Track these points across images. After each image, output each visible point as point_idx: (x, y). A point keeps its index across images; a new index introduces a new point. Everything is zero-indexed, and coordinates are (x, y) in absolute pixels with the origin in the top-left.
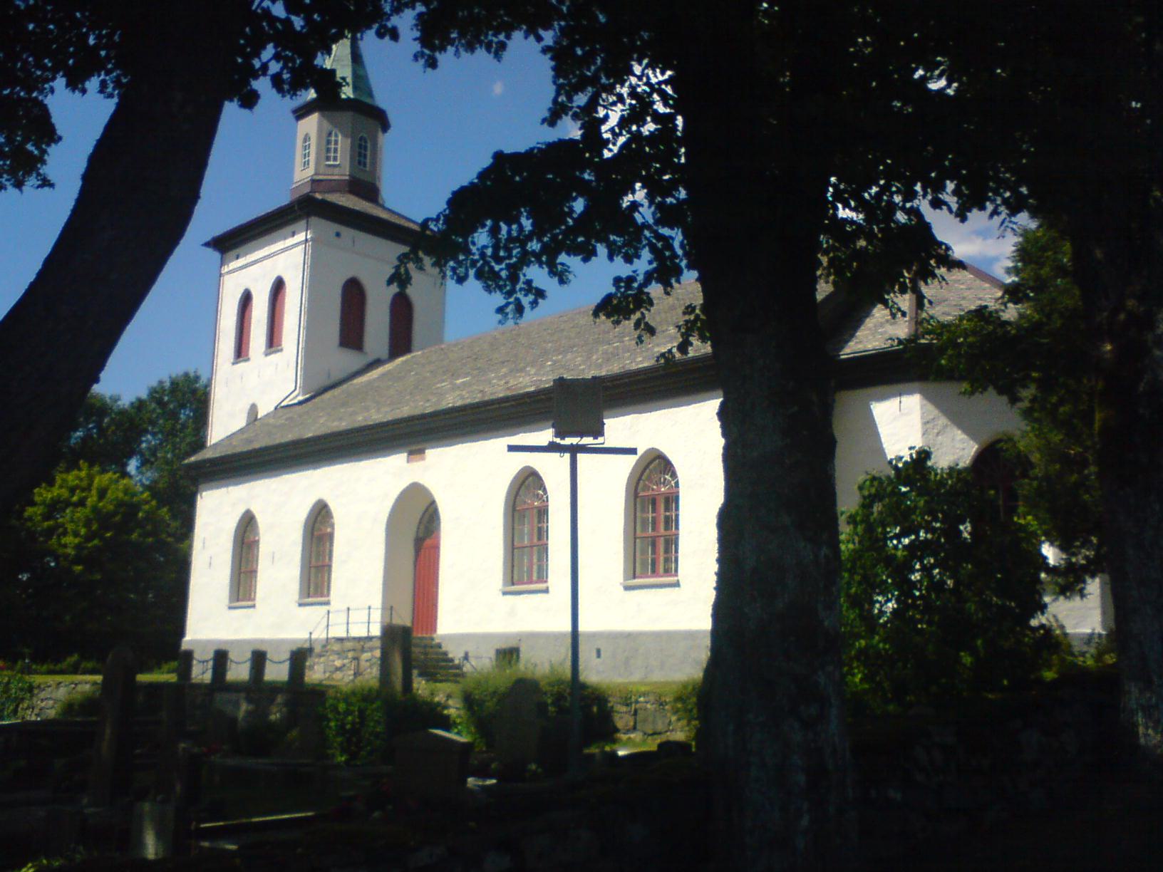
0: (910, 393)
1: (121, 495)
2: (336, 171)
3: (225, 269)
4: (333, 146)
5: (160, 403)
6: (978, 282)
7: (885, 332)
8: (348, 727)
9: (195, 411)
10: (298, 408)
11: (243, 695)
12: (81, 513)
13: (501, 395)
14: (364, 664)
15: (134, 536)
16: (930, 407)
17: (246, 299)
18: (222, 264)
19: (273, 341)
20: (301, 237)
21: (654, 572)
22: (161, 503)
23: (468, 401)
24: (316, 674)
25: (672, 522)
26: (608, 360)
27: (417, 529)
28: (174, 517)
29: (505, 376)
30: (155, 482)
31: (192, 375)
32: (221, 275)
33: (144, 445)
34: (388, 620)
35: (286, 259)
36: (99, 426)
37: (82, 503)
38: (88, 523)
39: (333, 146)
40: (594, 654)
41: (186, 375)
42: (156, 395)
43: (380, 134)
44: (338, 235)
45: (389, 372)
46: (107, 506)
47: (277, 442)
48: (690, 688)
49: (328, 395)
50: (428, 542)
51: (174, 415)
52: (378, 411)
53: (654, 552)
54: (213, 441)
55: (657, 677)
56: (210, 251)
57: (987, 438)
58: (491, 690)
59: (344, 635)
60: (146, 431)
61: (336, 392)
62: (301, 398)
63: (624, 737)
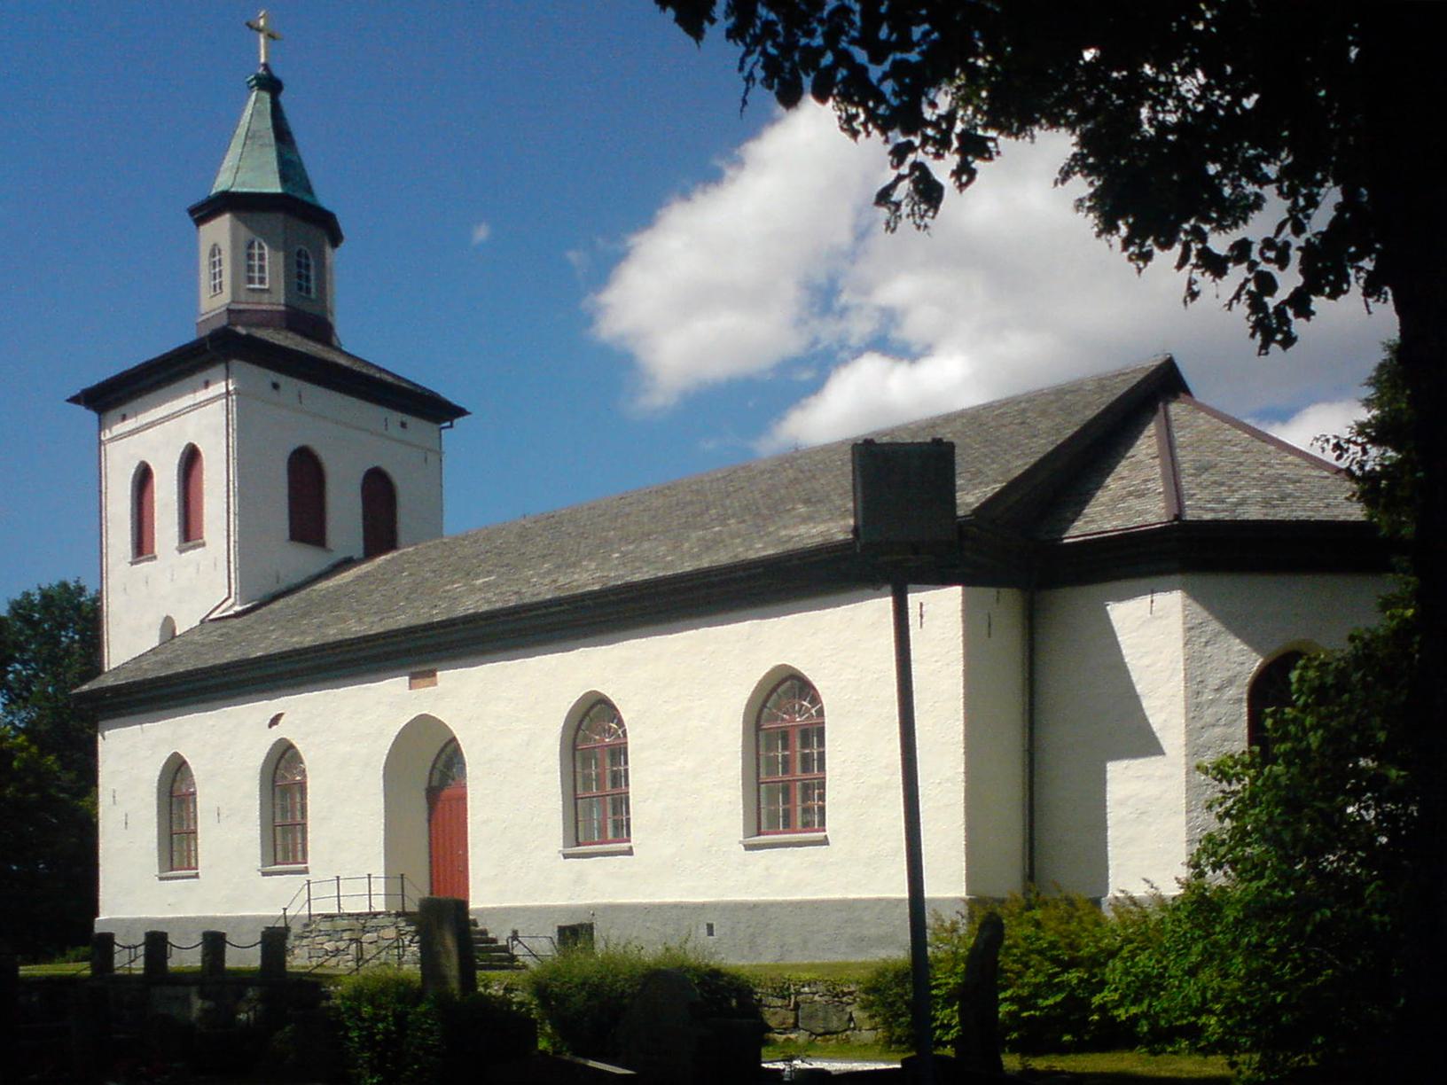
0: (1169, 589)
2: (266, 297)
3: (106, 435)
5: (27, 620)
6: (1258, 443)
7: (1129, 508)
9: (82, 633)
10: (236, 621)
11: (194, 989)
13: (549, 597)
16: (1196, 608)
17: (143, 477)
18: (101, 428)
19: (189, 532)
20: (219, 388)
21: (788, 826)
22: (45, 750)
23: (498, 605)
24: (299, 960)
26: (708, 548)
28: (66, 768)
29: (549, 572)
30: (32, 723)
31: (72, 585)
33: (11, 676)
34: (418, 891)
35: (200, 418)
40: (704, 931)
41: (64, 585)
43: (328, 250)
44: (276, 386)
45: (367, 574)
47: (210, 663)
48: (890, 975)
49: (276, 606)
50: (447, 792)
53: (786, 800)
54: (113, 666)
55: (797, 958)
56: (80, 409)
57: (1277, 646)
60: (12, 659)
62: (238, 608)
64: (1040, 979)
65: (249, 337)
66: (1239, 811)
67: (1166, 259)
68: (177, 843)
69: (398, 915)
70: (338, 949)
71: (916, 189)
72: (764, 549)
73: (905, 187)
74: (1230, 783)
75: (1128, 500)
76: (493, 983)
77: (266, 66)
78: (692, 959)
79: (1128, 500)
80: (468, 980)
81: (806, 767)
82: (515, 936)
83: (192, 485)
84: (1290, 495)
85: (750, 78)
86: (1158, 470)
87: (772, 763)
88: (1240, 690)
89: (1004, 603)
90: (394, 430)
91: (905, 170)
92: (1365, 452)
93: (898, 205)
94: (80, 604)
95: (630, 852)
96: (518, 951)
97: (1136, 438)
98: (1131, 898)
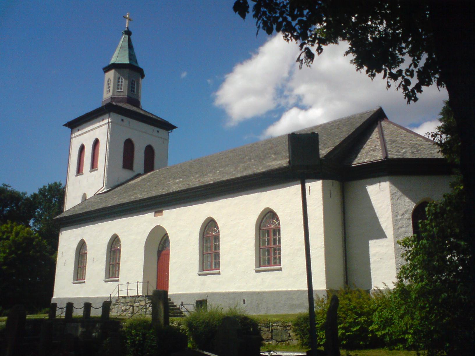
1: (25, 235)
2: (122, 94)
3: (73, 136)
4: (120, 83)
5: (44, 195)
6: (408, 134)
8: (137, 342)
9: (59, 200)
10: (104, 194)
11: (80, 324)
12: (7, 243)
13: (198, 185)
14: (136, 310)
15: (31, 253)
16: (393, 187)
17: (82, 148)
18: (72, 133)
19: (94, 166)
20: (106, 121)
21: (269, 264)
22: (44, 238)
23: (182, 188)
24: (114, 313)
25: (277, 241)
26: (245, 169)
27: (159, 247)
28: (49, 244)
29: (198, 177)
30: (41, 229)
31: (58, 183)
32: (71, 138)
33: (36, 213)
34: (153, 287)
35: (100, 131)
36: (17, 205)
37: (8, 238)
38: (10, 247)
39: (120, 83)
40: (242, 302)
41: (56, 183)
42: (42, 191)
43: (140, 79)
45: (144, 179)
46: (19, 239)
48: (302, 319)
50: (163, 252)
51: (50, 201)
52: (141, 194)
53: (268, 255)
55: (272, 312)
58: (201, 321)
59: (126, 295)
60: (38, 208)
61: (121, 187)
62: (106, 190)
63: (267, 343)
64: (351, 320)
65: (116, 105)
66: (412, 257)
67: (379, 76)
68: (79, 273)
69: (146, 296)
70: (126, 309)
71: (307, 55)
72: (262, 169)
73: (303, 55)
74: (408, 247)
75: (370, 153)
76: (175, 322)
77: (128, 28)
78: (238, 313)
79: (370, 153)
80: (167, 321)
81: (275, 243)
82: (182, 305)
83: (96, 150)
84: (420, 150)
85: (259, 27)
86: (379, 143)
87: (264, 241)
88: (409, 215)
89: (334, 185)
90: (155, 133)
91: (303, 50)
92: (441, 137)
93: (302, 60)
94: (60, 189)
95: (219, 273)
96: (183, 310)
97: (372, 132)
98: (379, 290)
